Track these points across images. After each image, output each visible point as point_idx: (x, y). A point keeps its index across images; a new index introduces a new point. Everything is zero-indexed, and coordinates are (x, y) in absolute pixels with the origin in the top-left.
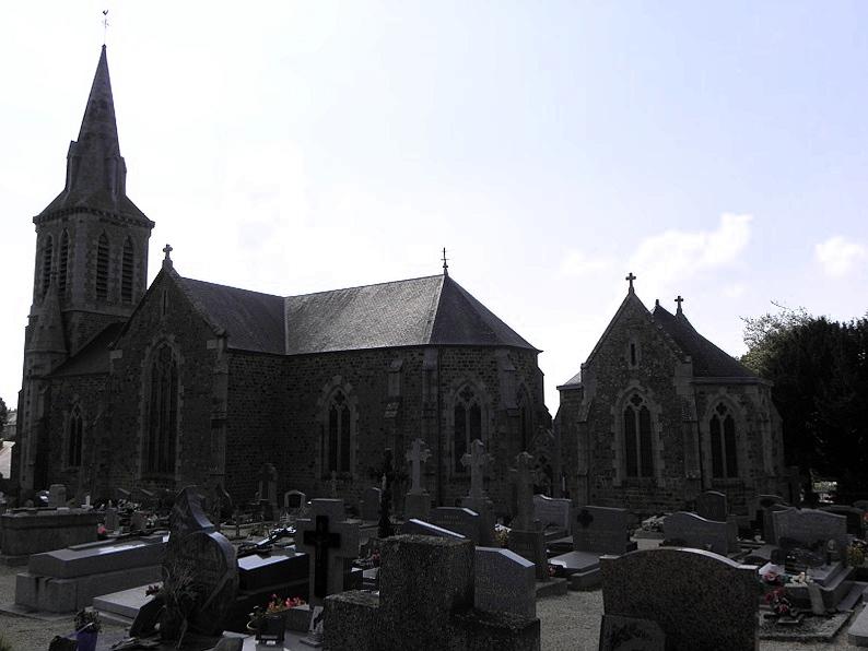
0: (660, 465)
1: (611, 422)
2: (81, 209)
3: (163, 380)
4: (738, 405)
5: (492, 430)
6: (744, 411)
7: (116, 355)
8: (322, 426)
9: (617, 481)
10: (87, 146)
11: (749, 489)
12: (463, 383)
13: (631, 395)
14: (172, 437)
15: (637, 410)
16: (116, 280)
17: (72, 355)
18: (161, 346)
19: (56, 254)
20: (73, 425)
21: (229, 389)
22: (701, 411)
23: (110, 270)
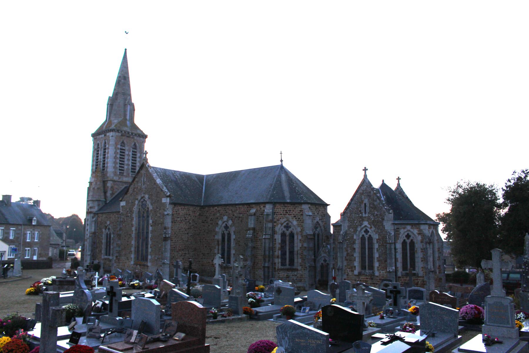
0: (376, 264)
1: (354, 243)
2: (112, 130)
3: (143, 217)
4: (417, 235)
5: (300, 245)
6: (420, 238)
7: (123, 204)
8: (218, 241)
9: (356, 272)
10: (116, 99)
11: (421, 277)
12: (285, 221)
13: (364, 229)
14: (147, 244)
15: (367, 236)
16: (128, 165)
17: (108, 202)
18: (142, 200)
19: (101, 152)
20: (107, 237)
21: (172, 222)
22: (396, 236)
23: (126, 160)
